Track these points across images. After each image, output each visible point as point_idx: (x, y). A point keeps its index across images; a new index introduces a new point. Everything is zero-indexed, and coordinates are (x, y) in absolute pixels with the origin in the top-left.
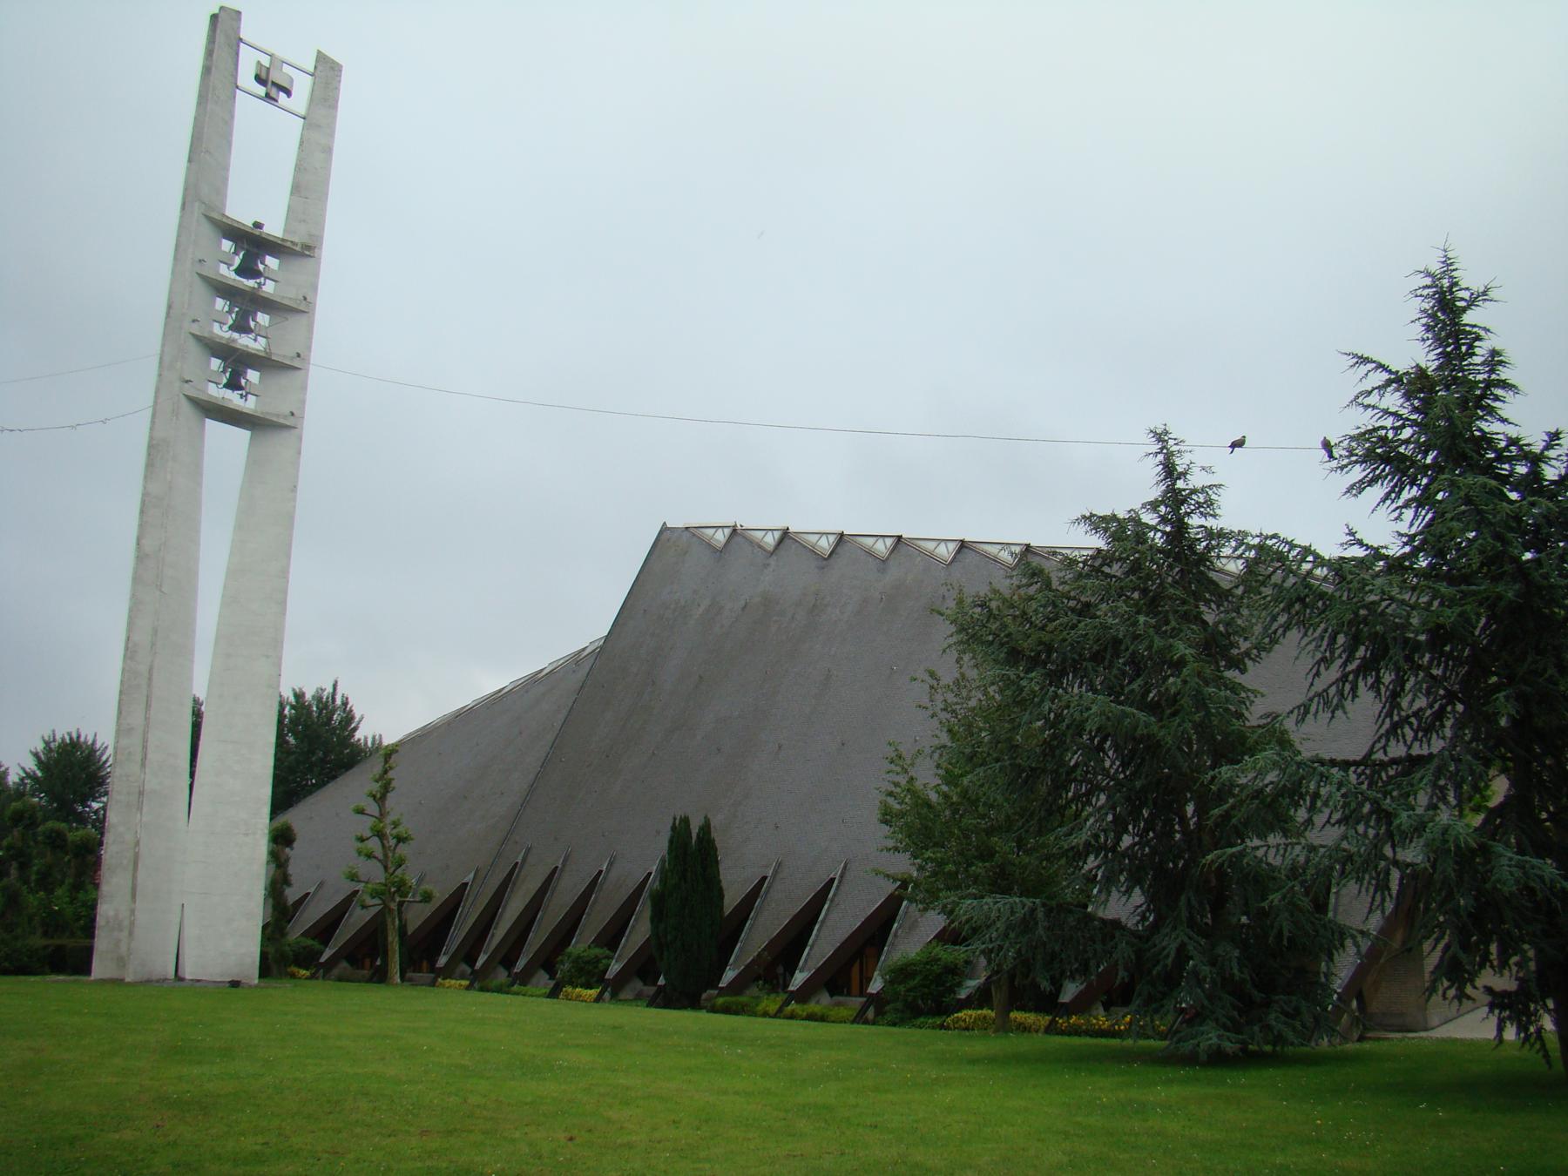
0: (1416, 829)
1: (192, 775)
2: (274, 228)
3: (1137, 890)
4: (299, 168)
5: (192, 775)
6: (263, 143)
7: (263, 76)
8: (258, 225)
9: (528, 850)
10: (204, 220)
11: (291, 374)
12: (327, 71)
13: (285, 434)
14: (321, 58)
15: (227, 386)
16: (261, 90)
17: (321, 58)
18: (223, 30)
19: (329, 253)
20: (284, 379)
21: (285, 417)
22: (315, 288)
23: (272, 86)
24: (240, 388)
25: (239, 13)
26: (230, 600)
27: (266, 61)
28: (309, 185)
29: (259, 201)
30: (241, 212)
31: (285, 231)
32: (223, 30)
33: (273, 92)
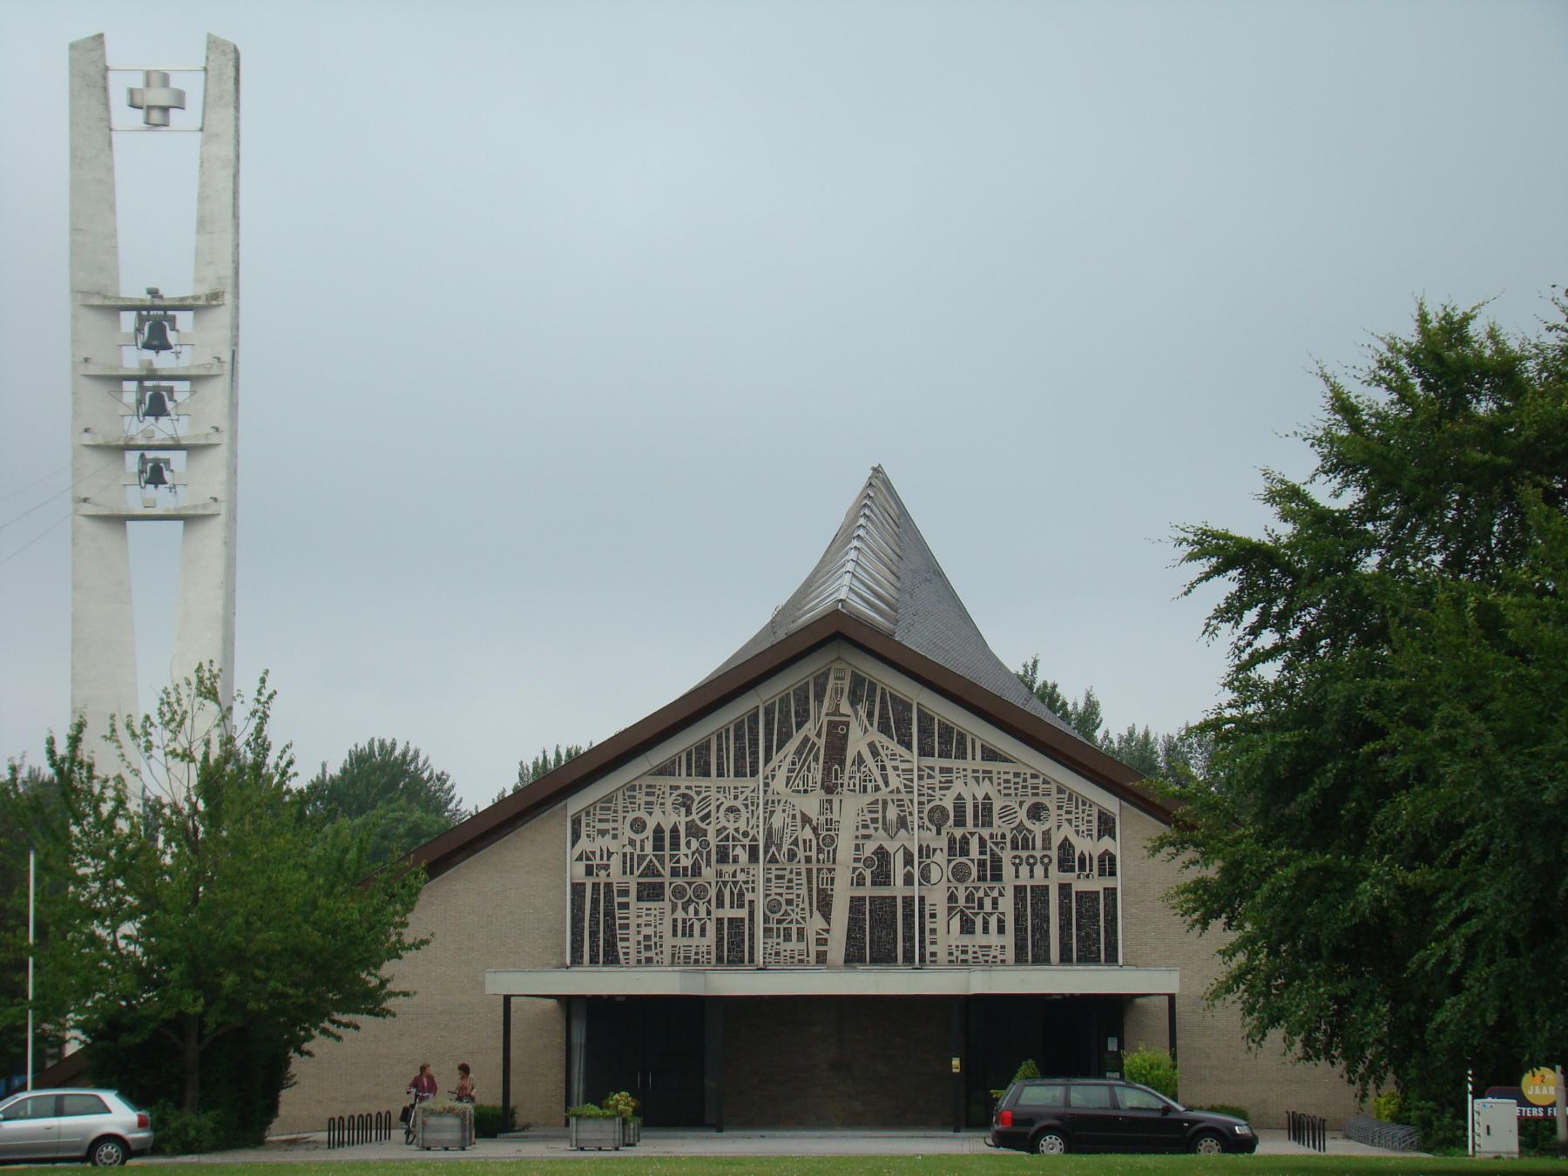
6: (157, 179)
7: (138, 101)
10: (84, 311)
15: (147, 346)
17: (213, 44)
18: (89, 64)
21: (205, 506)
25: (101, 36)
27: (138, 82)
28: (222, 210)
29: (157, 261)
32: (89, 64)
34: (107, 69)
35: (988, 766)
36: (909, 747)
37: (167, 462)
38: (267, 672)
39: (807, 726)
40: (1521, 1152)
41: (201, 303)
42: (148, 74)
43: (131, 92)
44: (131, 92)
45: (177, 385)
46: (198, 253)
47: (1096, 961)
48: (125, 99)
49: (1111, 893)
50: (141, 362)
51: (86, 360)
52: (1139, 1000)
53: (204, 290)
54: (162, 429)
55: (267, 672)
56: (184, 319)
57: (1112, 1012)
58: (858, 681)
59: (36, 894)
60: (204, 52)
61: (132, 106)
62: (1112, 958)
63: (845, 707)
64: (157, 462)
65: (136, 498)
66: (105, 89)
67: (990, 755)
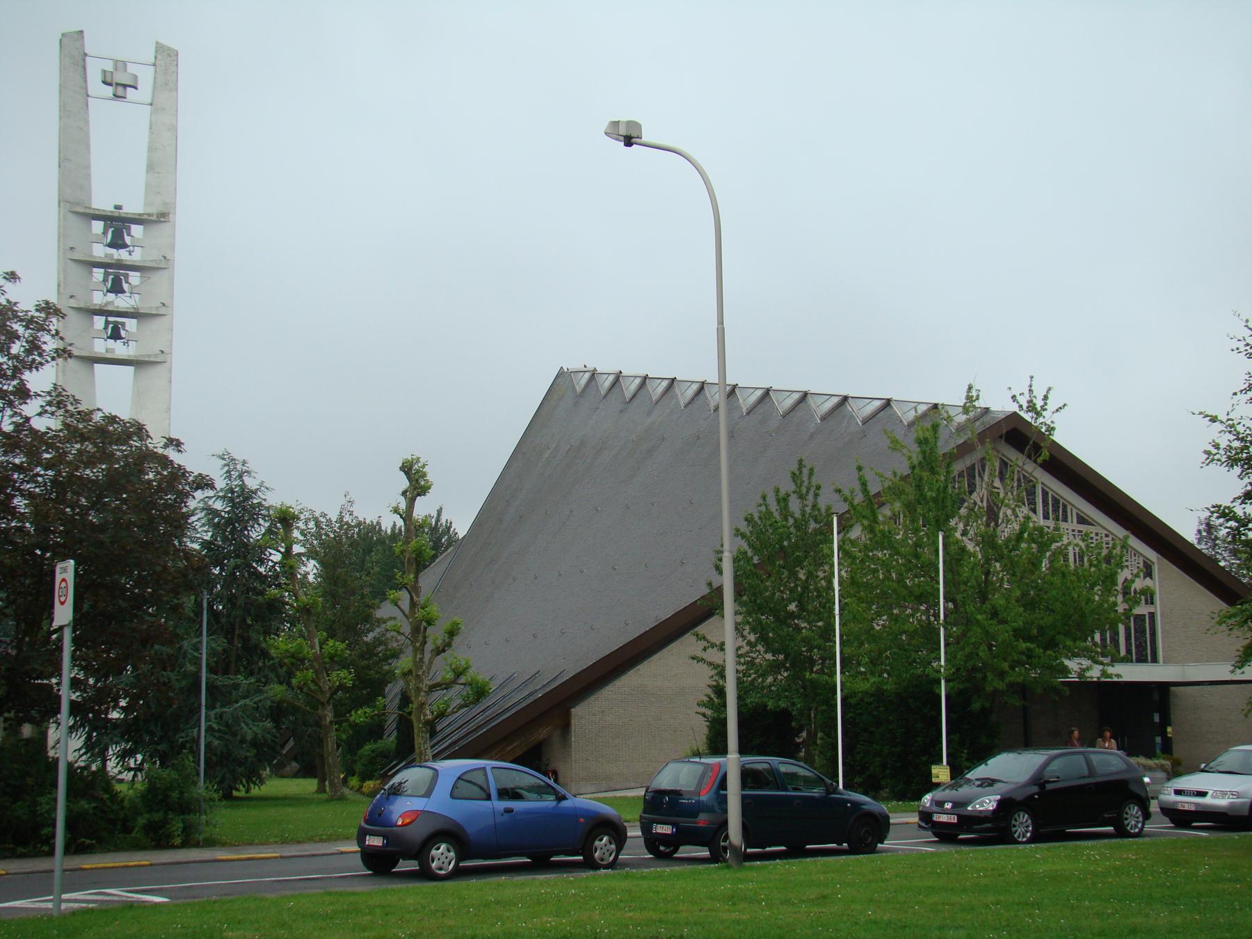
0: (959, 560)
1: (721, 322)
2: (133, 206)
3: (379, 614)
4: (152, 149)
5: (721, 322)
6: (118, 133)
7: (109, 80)
8: (118, 207)
9: (452, 633)
10: (70, 215)
11: (158, 321)
12: (166, 57)
13: (159, 368)
14: (160, 48)
15: (111, 245)
16: (109, 91)
17: (160, 48)
18: (73, 50)
19: (181, 217)
20: (154, 324)
21: (156, 355)
22: (173, 248)
23: (119, 87)
24: (125, 246)
25: (82, 32)
26: (8, 908)
27: (109, 67)
28: (160, 162)
29: (117, 185)
30: (102, 202)
31: (146, 204)
32: (73, 50)
33: (120, 91)
34: (86, 55)
35: (1083, 528)
36: (1034, 511)
37: (123, 324)
38: (1050, 389)
39: (975, 494)
40: (952, 778)
41: (154, 218)
42: (116, 62)
43: (104, 72)
44: (104, 72)
45: (131, 273)
46: (148, 186)
47: (1145, 661)
48: (99, 78)
49: (1152, 615)
50: (106, 256)
51: (72, 248)
52: (1173, 689)
53: (153, 210)
54: (120, 303)
55: (1050, 389)
56: (137, 230)
57: (1158, 696)
58: (1004, 464)
59: (944, 562)
60: (153, 54)
61: (104, 82)
62: (1155, 660)
63: (997, 483)
64: (116, 324)
65: (101, 347)
66: (85, 68)
67: (1082, 520)
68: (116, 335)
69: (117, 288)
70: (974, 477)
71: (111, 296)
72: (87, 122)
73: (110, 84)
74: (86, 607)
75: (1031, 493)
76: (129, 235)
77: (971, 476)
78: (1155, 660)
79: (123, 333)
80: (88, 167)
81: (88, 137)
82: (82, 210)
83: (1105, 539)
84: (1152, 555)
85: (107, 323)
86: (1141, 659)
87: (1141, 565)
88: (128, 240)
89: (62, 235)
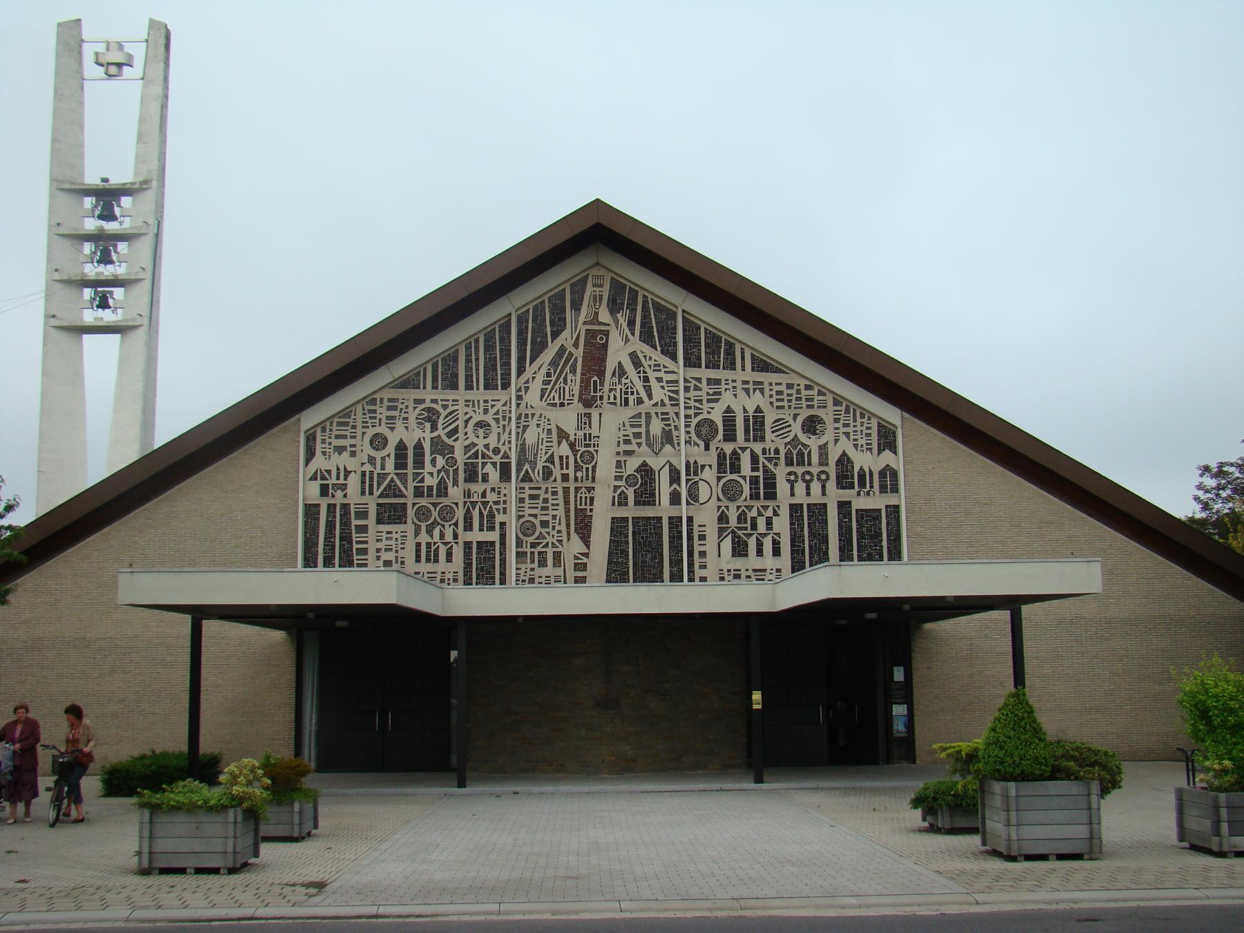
7: (101, 61)
8: (105, 180)
12: (161, 39)
15: (101, 217)
21: (133, 320)
23: (115, 68)
25: (79, 20)
27: (101, 48)
29: (110, 157)
30: (92, 179)
32: (70, 36)
35: (759, 377)
39: (566, 334)
41: (137, 186)
43: (97, 54)
44: (97, 54)
46: (137, 156)
61: (97, 63)
62: (895, 555)
63: (604, 315)
65: (90, 316)
66: (80, 53)
67: (762, 365)
68: (104, 305)
69: (106, 259)
70: (563, 310)
71: (101, 268)
72: (82, 104)
73: (102, 65)
74: (907, 607)
75: (667, 334)
76: (119, 206)
77: (558, 310)
78: (895, 555)
79: (111, 302)
80: (82, 146)
81: (82, 118)
82: (67, 186)
83: (804, 393)
84: (892, 414)
85: (96, 293)
86: (870, 554)
87: (874, 432)
88: (117, 211)
89: (51, 211)
